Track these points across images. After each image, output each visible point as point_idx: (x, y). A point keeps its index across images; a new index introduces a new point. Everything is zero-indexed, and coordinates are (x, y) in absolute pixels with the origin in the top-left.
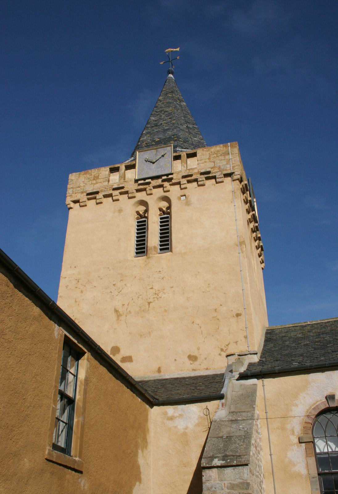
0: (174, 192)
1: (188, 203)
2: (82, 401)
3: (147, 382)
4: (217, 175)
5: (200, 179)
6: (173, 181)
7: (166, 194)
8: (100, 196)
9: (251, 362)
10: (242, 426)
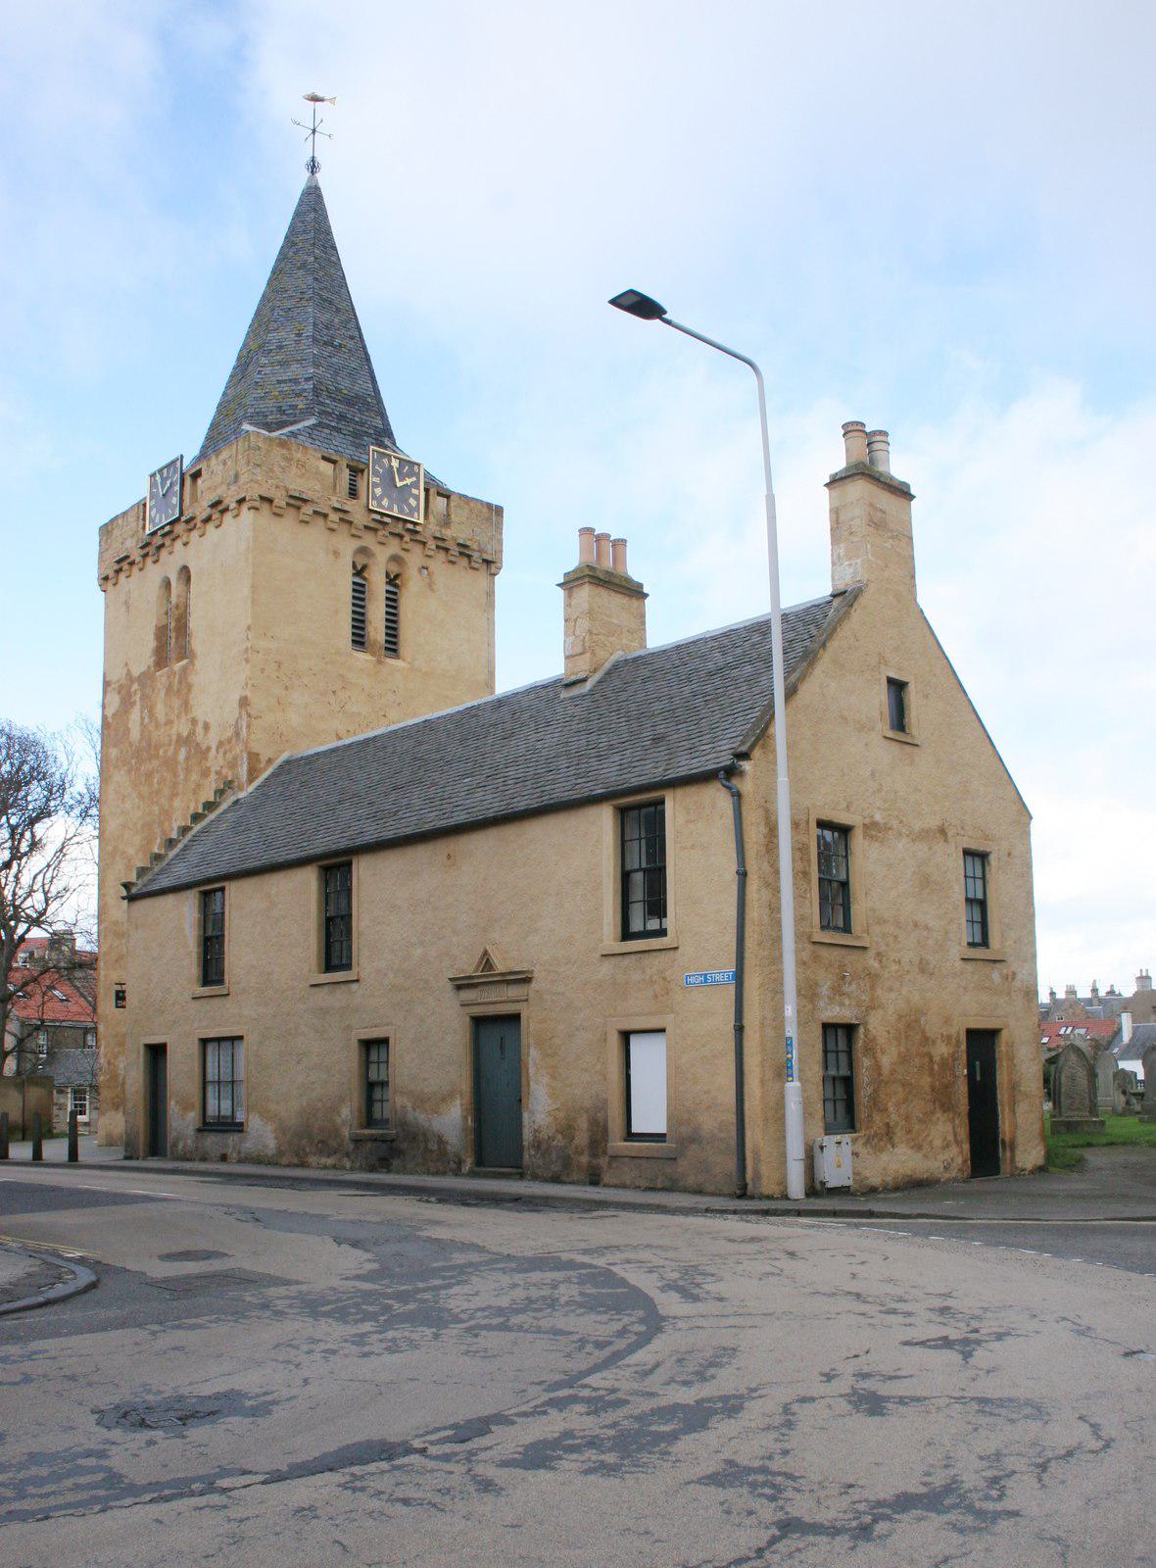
0: (415, 558)
1: (430, 586)
2: (629, 658)
3: (516, 694)
4: (476, 555)
5: (453, 553)
6: (418, 537)
7: (403, 554)
8: (308, 509)
9: (316, 969)
10: (386, 499)
